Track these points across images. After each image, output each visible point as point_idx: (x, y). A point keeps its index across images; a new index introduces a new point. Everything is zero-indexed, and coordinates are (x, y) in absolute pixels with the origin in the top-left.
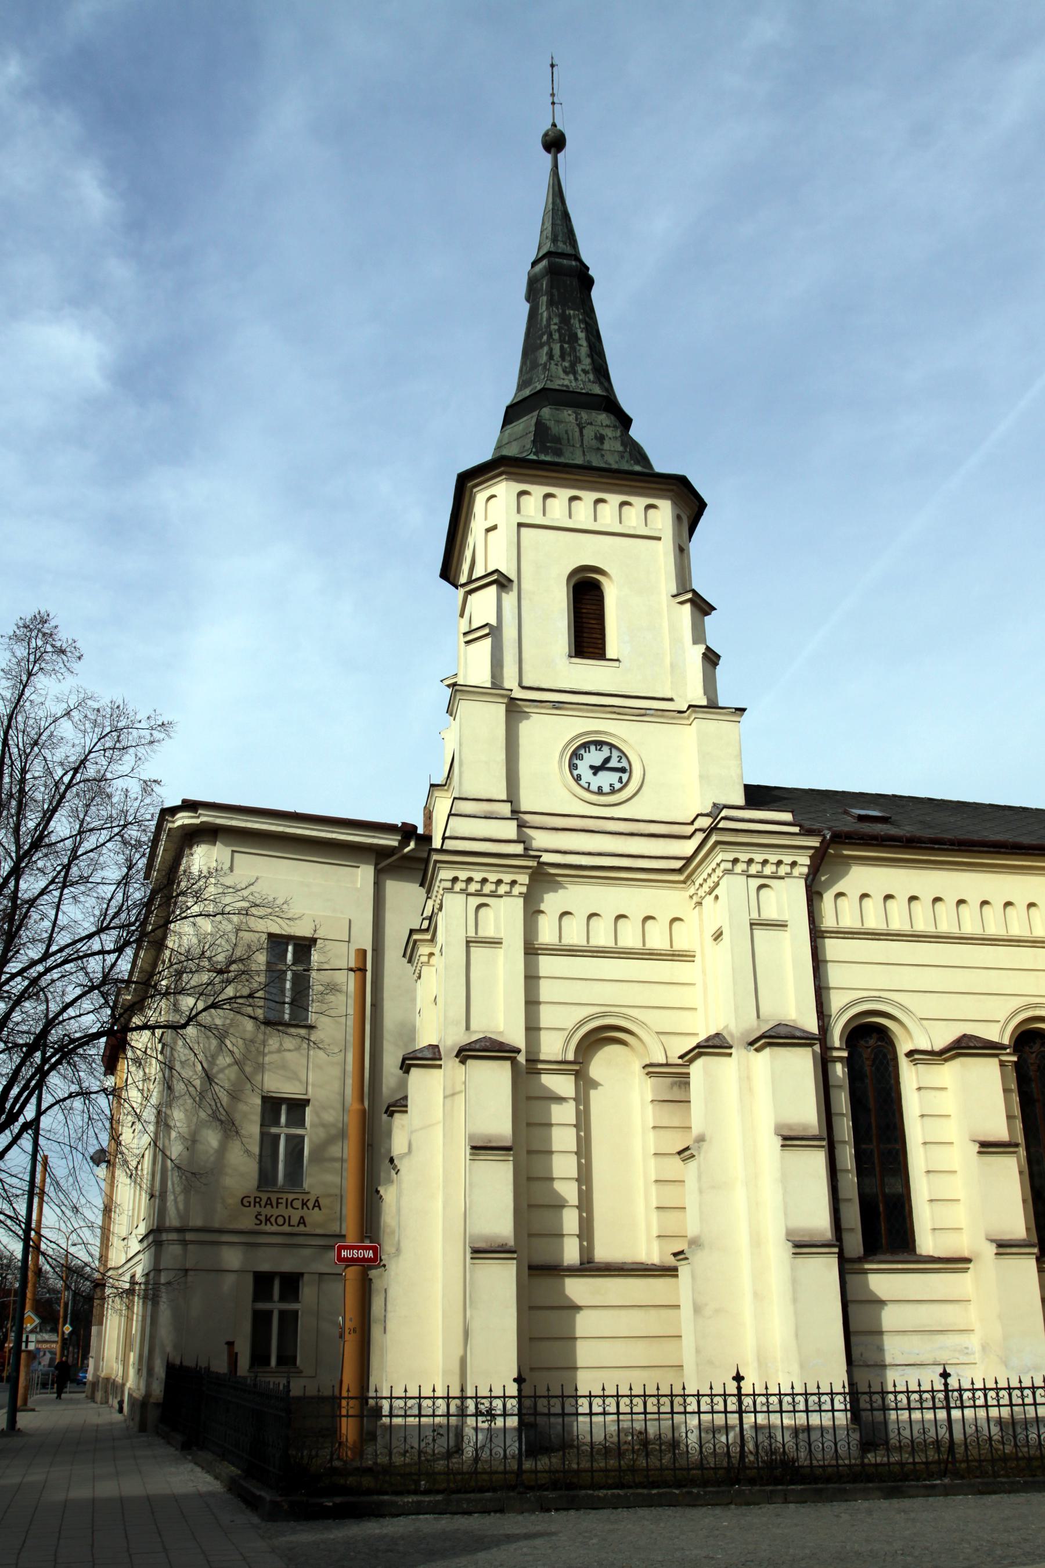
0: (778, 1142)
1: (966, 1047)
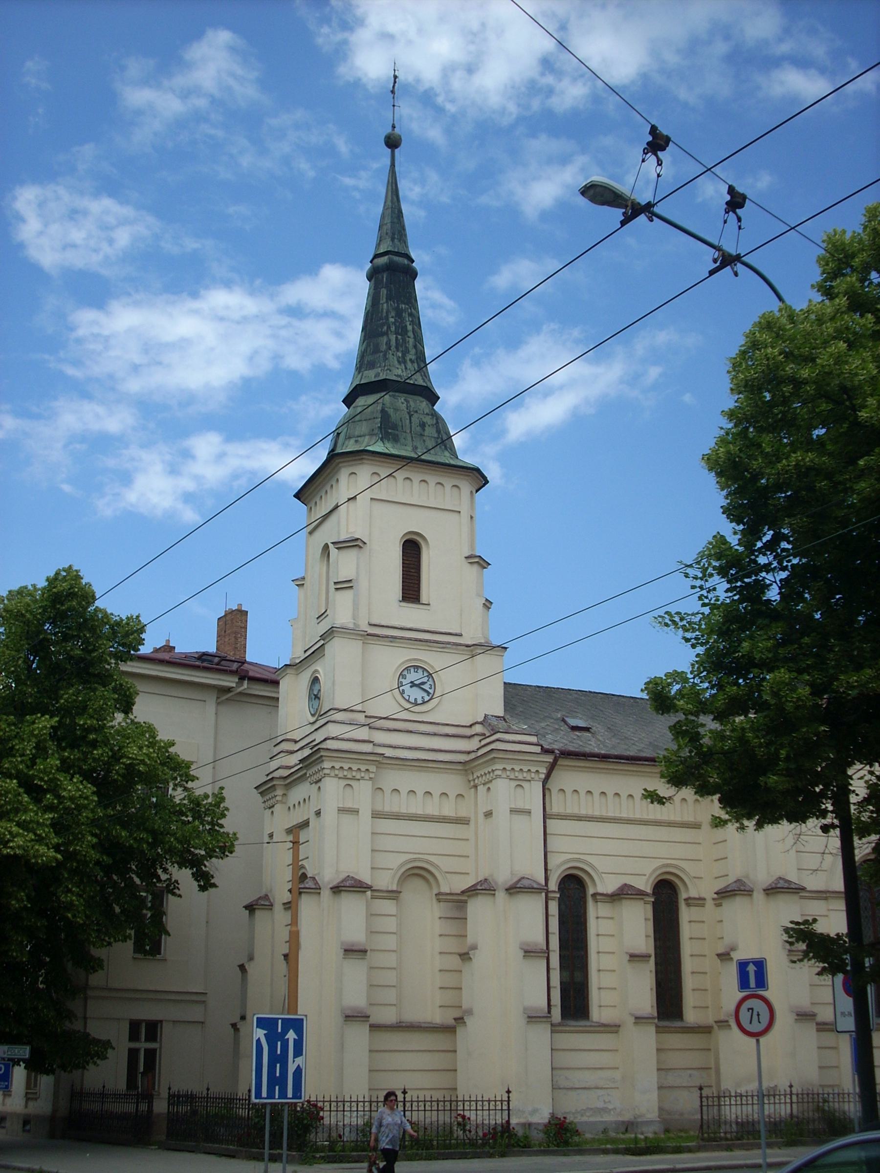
0: (522, 953)
1: (624, 893)
